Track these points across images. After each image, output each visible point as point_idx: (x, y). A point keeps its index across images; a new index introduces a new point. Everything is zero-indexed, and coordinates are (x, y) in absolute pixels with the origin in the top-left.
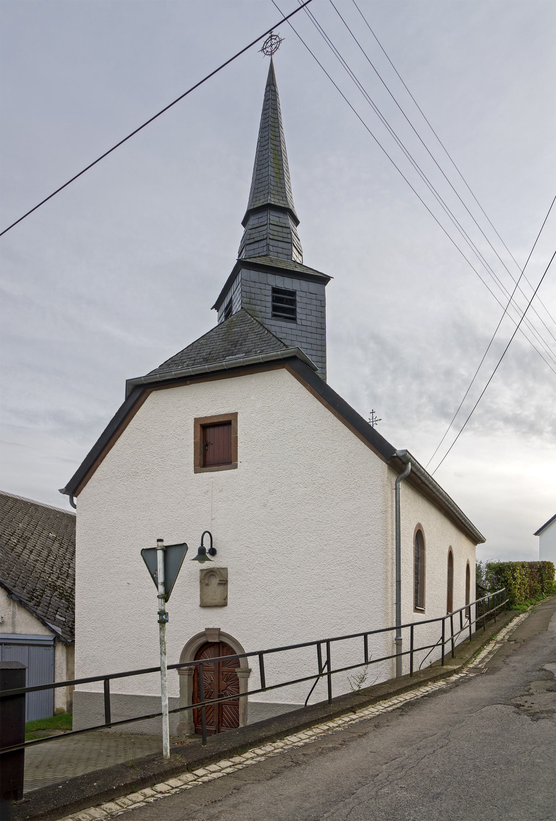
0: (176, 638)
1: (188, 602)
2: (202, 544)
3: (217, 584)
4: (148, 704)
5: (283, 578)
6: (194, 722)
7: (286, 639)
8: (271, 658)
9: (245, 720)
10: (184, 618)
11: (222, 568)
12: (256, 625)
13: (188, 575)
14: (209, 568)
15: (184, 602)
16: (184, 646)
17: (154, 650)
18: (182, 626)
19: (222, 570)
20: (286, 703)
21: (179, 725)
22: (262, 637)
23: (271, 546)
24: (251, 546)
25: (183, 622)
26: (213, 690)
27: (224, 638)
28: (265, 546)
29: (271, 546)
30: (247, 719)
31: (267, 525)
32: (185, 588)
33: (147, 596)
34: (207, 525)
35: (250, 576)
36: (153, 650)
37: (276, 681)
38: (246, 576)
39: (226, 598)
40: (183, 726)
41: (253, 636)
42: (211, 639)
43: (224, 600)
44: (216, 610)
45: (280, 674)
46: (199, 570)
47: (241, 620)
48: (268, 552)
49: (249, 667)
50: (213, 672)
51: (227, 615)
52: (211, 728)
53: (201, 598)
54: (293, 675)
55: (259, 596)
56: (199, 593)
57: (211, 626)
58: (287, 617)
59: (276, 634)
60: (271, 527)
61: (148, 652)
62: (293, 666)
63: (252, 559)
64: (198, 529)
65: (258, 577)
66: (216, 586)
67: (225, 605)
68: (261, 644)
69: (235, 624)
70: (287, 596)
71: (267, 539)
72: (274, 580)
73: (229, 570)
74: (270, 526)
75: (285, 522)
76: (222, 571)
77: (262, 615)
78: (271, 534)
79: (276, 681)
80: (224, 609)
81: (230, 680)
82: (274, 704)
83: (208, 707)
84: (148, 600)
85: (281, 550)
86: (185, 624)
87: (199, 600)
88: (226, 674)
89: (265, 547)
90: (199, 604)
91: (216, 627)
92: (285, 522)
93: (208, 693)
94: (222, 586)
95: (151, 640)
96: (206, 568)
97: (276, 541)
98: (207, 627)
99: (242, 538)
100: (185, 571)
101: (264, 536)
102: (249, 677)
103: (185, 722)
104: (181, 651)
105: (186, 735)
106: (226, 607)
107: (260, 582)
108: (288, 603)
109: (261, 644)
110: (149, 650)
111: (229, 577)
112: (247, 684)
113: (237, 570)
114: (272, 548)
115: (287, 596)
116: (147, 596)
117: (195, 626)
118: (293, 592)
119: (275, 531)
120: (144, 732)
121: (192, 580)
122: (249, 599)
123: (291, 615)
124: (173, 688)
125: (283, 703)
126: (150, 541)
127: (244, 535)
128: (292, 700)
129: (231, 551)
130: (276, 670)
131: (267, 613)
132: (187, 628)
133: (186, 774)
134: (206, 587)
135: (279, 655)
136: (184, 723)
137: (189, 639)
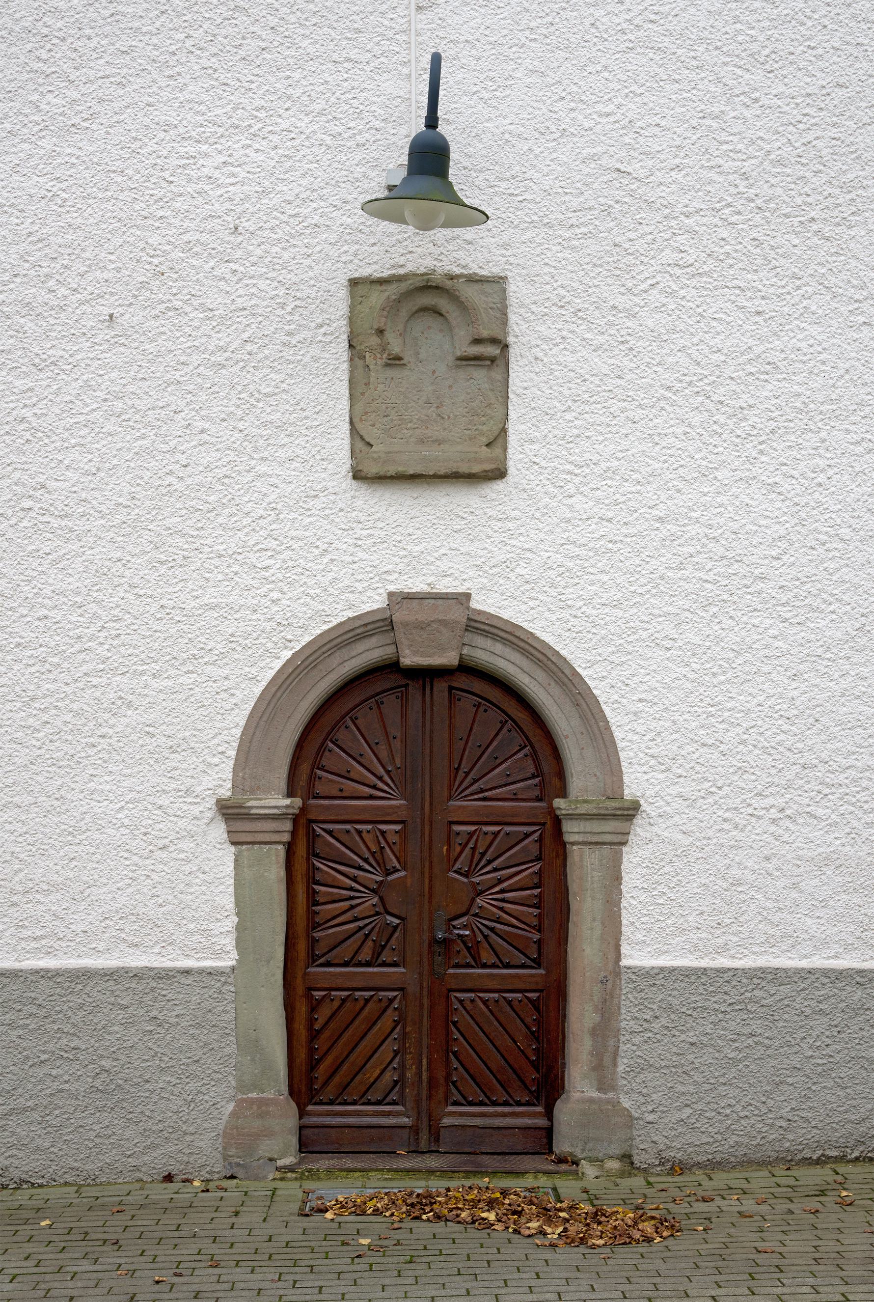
0: (211, 644)
1: (281, 454)
2: (432, 121)
3: (451, 359)
4: (42, 1013)
5: (803, 345)
6: (292, 1092)
7: (820, 651)
8: (743, 742)
9: (607, 1060)
10: (255, 538)
11: (473, 280)
12: (662, 578)
13: (283, 306)
14: (402, 271)
15: (256, 449)
16: (258, 690)
17: (77, 714)
18: (246, 579)
19: (477, 287)
20: (818, 962)
21: (234, 1114)
22: (697, 640)
23: (745, 176)
24: (634, 168)
25: (253, 558)
26: (397, 921)
27: (488, 643)
28: (713, 175)
29: (745, 176)
30: (616, 1054)
31: (725, 64)
32: (259, 374)
33: (27, 413)
34: (390, 34)
35: (630, 324)
36: (68, 717)
37: (767, 859)
38: (611, 324)
39: (499, 438)
40: (261, 1116)
41: (645, 634)
42: (415, 653)
44: (444, 501)
45: (787, 823)
46: (343, 279)
47: (583, 552)
48: (729, 205)
49: (628, 793)
50: (398, 827)
51: (510, 525)
52: (389, 1114)
54: (855, 823)
55: (679, 430)
56: (344, 404)
57: (418, 585)
58: (823, 538)
59: (769, 622)
60: (747, 76)
61: (37, 724)
62: (854, 780)
63: (642, 236)
64: (335, 57)
65: (674, 331)
66: (442, 369)
67: (499, 474)
68: (692, 676)
69: (552, 574)
70: (823, 434)
71: (724, 136)
72: (758, 350)
73: (516, 290)
74: (739, 72)
75: (819, 57)
76: (469, 293)
77: (693, 530)
78: (747, 113)
79: (767, 859)
81: (489, 862)
82: (763, 970)
83: (370, 1005)
84: (28, 435)
85: (799, 201)
86: (267, 568)
88: (471, 834)
89: (711, 182)
91: (445, 586)
92: (819, 57)
93: (367, 936)
94: (480, 374)
95: (56, 660)
96: (386, 274)
97: (769, 152)
98: (392, 588)
100: (262, 284)
101: (708, 122)
102: (624, 843)
103: (269, 1095)
104: (239, 718)
105: (280, 1163)
106: (499, 486)
107: (682, 358)
108: (830, 472)
109: (692, 676)
110: (45, 717)
112: (617, 878)
113: (562, 292)
114: (750, 186)
115: (823, 434)
116: (27, 413)
117: (325, 581)
118: (853, 418)
119: (764, 101)
120: (16, 1174)
122: (625, 444)
123: (845, 532)
124: (193, 919)
125: (804, 964)
126: (35, 97)
127: (600, 107)
128: (848, 948)
130: (770, 801)
131: (721, 521)
132: (275, 595)
134: (391, 373)
135: (785, 727)
136: (262, 1102)
137: (287, 654)
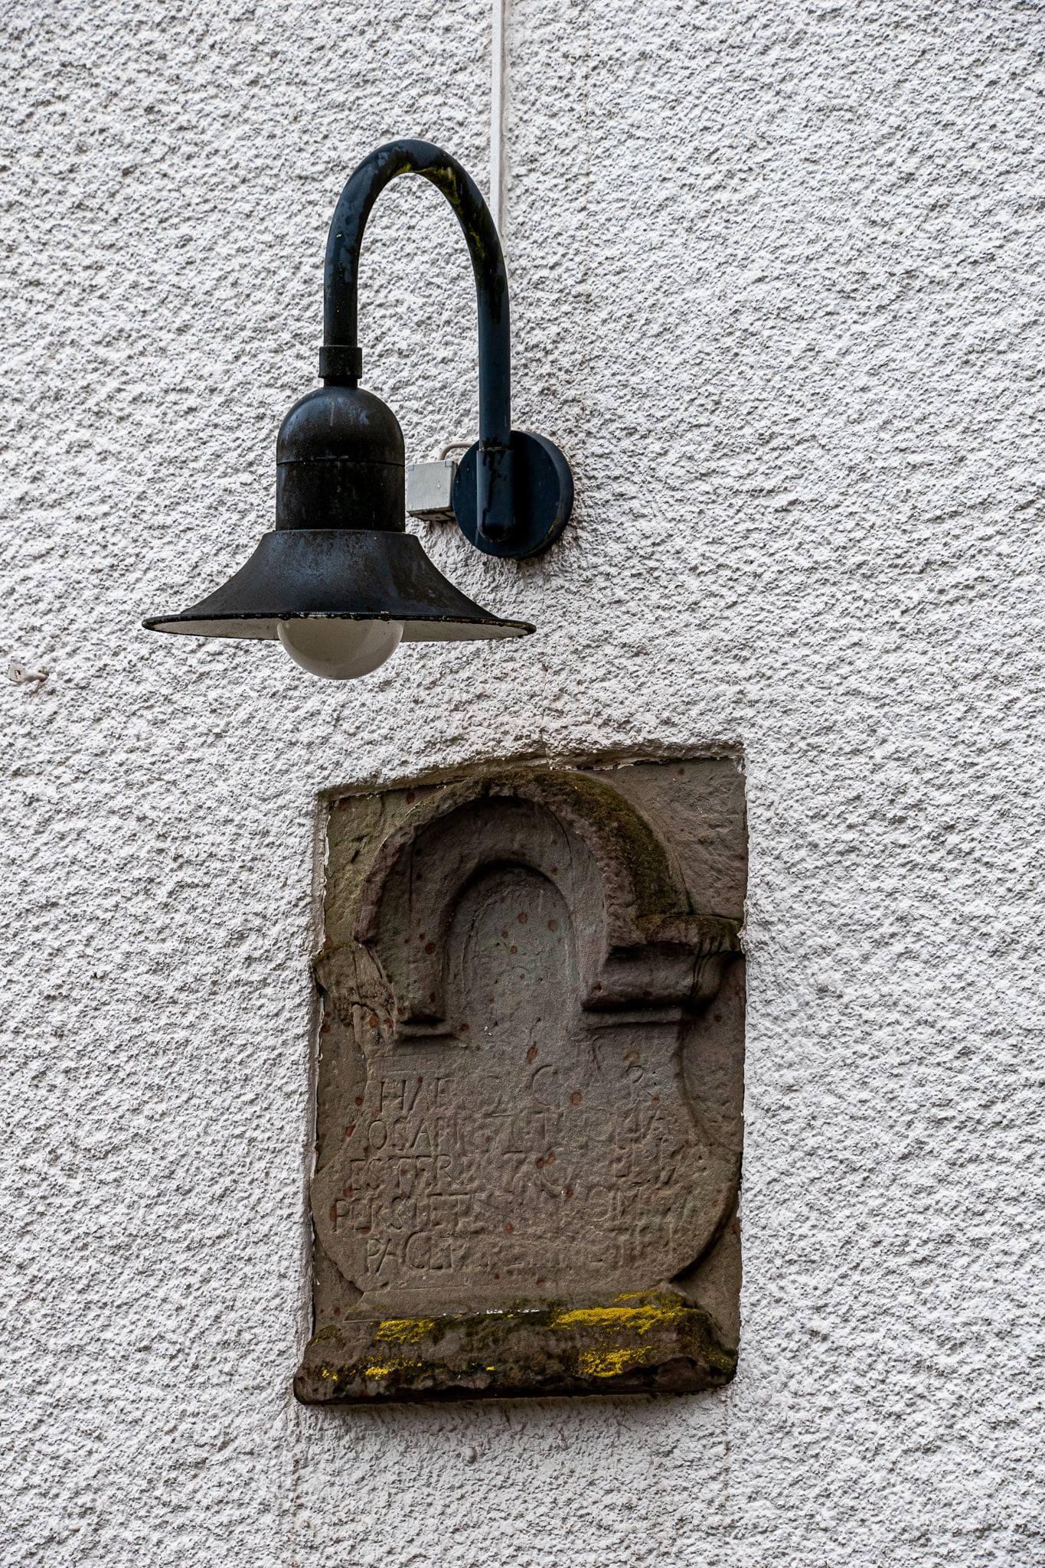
1: (122, 1333)
14: (455, 756)
19: (669, 779)
34: (440, 73)
43: (685, 1277)
46: (300, 792)
53: (316, 1253)
64: (303, 164)
80: (690, 1448)
87: (294, 1289)
90: (294, 1361)
99: (979, 246)
100: (99, 830)
111: (759, 900)
113: (894, 774)
121: (202, 963)
129: (804, 465)
133: (704, 1399)
